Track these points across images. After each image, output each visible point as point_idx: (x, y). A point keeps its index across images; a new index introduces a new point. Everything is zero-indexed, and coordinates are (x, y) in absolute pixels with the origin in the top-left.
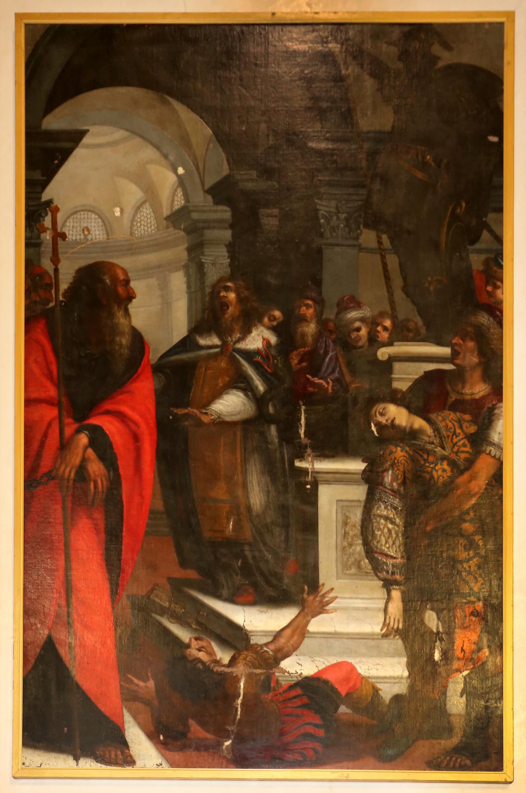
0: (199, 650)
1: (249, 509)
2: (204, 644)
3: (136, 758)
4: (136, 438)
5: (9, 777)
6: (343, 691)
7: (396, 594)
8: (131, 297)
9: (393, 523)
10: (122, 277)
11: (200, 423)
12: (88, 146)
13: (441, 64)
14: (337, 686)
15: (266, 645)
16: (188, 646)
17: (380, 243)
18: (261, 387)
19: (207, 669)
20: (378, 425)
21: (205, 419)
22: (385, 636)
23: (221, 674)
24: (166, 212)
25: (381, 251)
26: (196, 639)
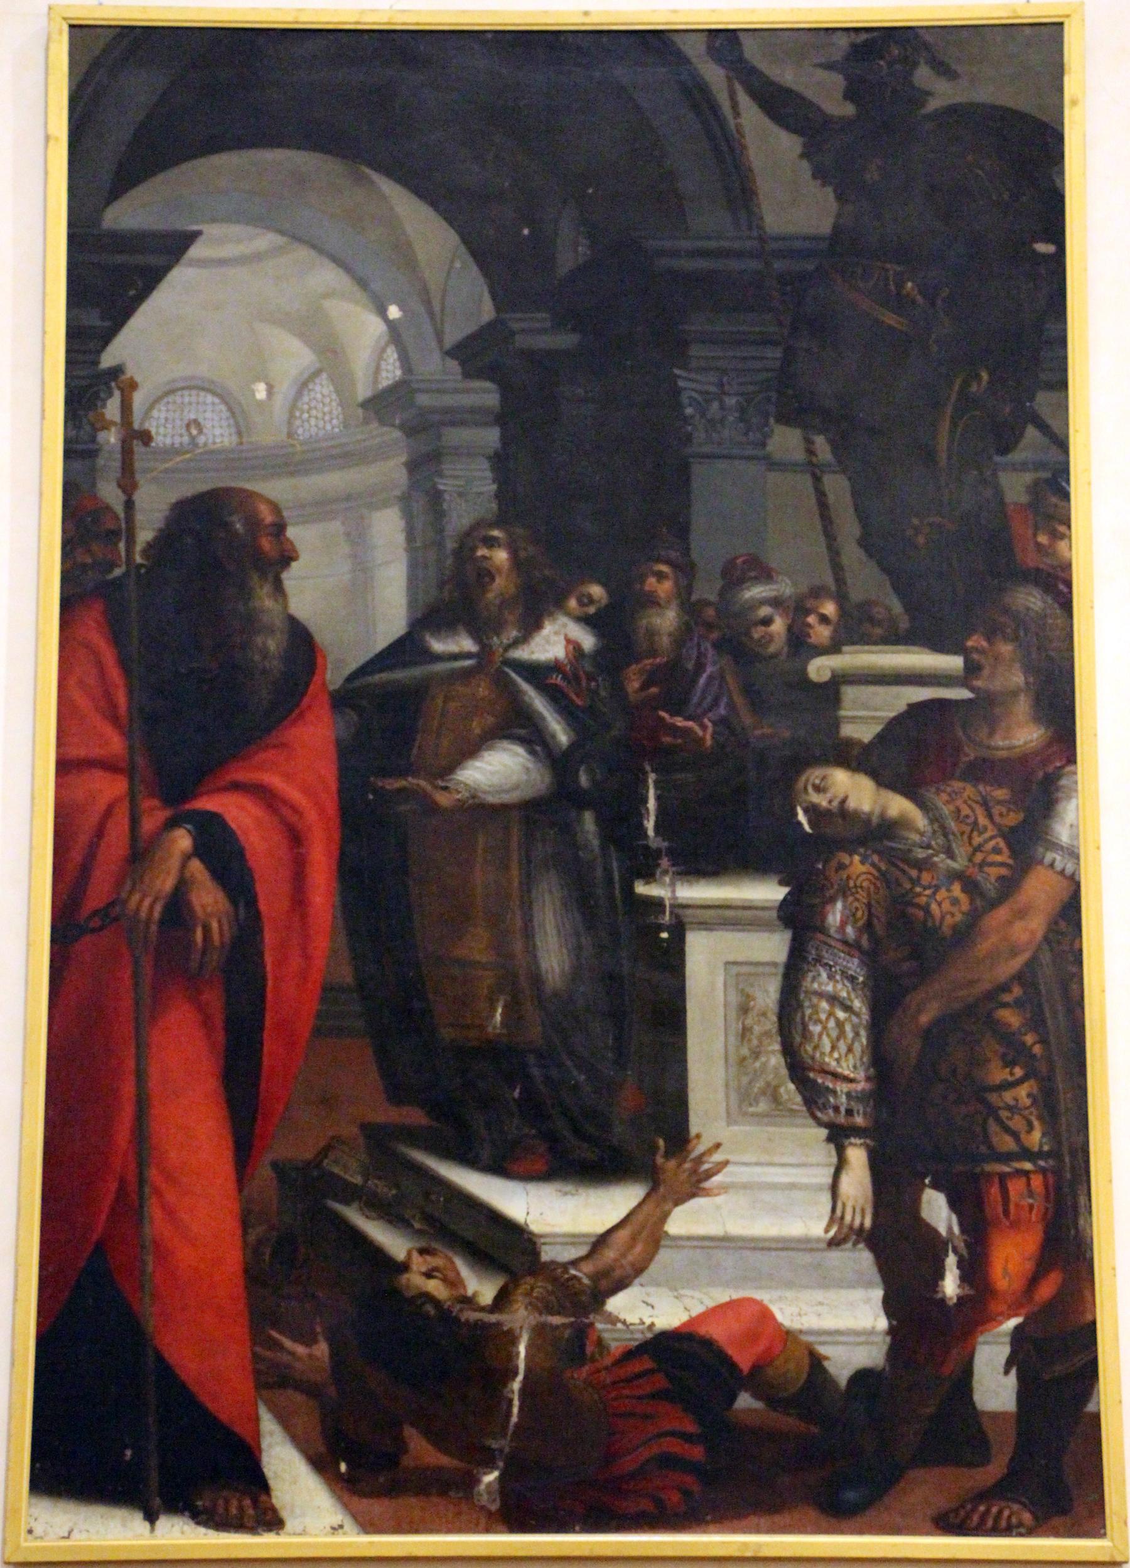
0: (428, 1275)
1: (537, 979)
3: (284, 1514)
4: (296, 838)
6: (744, 1361)
7: (857, 1156)
8: (287, 557)
9: (848, 1008)
10: (269, 519)
11: (433, 808)
13: (933, 105)
15: (574, 1263)
16: (404, 1267)
17: (811, 452)
19: (445, 1316)
21: (443, 800)
22: (834, 1243)
24: (363, 392)
25: (815, 472)
26: (422, 1252)
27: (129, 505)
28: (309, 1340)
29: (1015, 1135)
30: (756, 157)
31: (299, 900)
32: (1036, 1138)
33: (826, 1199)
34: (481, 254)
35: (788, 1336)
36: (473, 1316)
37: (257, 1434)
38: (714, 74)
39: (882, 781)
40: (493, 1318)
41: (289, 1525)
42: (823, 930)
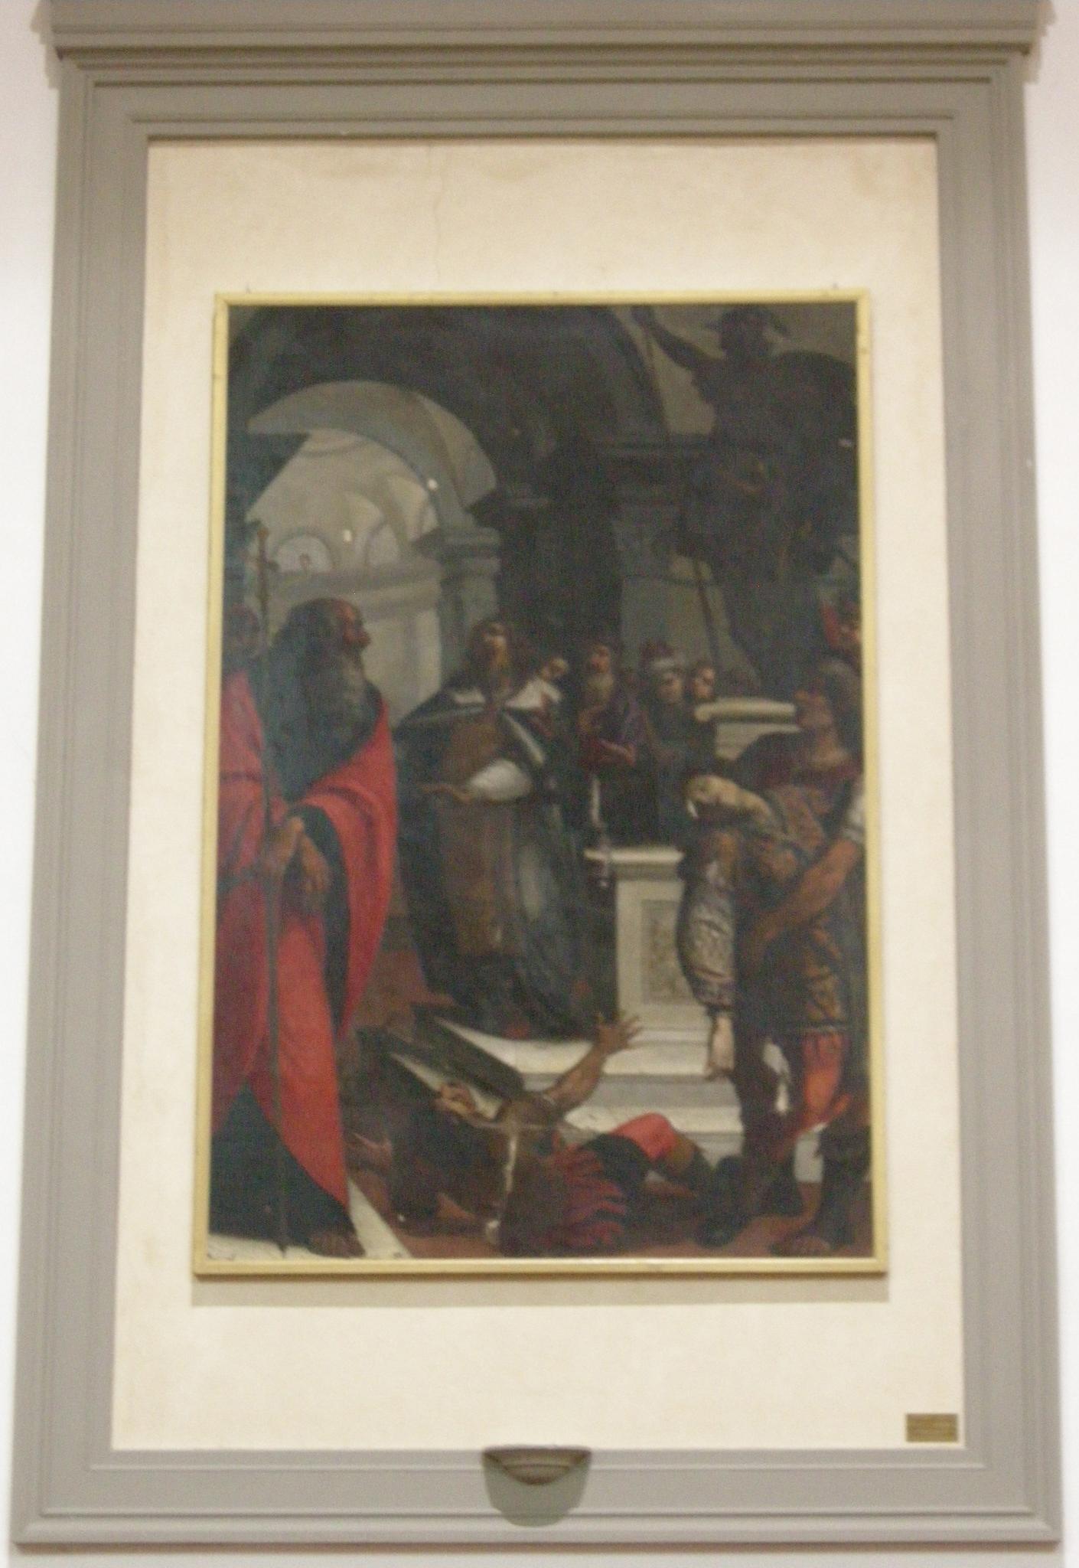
0: (454, 1099)
1: (523, 913)
2: (458, 1091)
3: (365, 1247)
4: (370, 823)
5: (184, 1282)
6: (652, 1150)
7: (725, 1023)
8: (363, 641)
9: (718, 929)
10: (352, 618)
11: (456, 803)
12: (315, 455)
13: (776, 352)
14: (643, 1146)
15: (546, 1092)
16: (439, 1095)
17: (698, 573)
18: (538, 755)
19: (464, 1124)
20: (701, 806)
21: (463, 797)
22: (710, 1078)
23: (485, 1131)
24: (412, 535)
25: (700, 586)
26: (452, 1085)
27: (264, 609)
28: (379, 1140)
29: (822, 1008)
30: (663, 384)
31: (372, 864)
32: (837, 1011)
33: (703, 1052)
34: (488, 445)
35: (679, 1138)
36: (482, 1125)
37: (347, 1198)
38: (636, 332)
39: (743, 784)
40: (493, 1126)
41: (370, 1252)
42: (704, 880)
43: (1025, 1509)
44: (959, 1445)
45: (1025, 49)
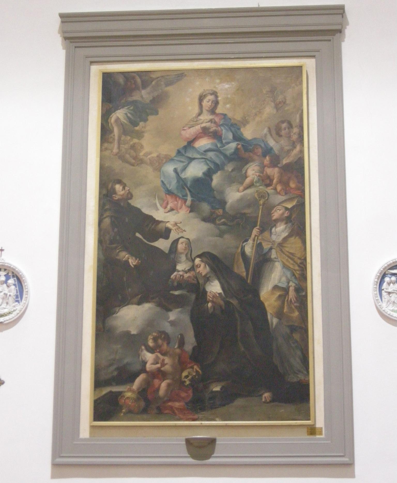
15: (208, 305)
43: (342, 454)
44: (323, 436)
45: (340, 31)
